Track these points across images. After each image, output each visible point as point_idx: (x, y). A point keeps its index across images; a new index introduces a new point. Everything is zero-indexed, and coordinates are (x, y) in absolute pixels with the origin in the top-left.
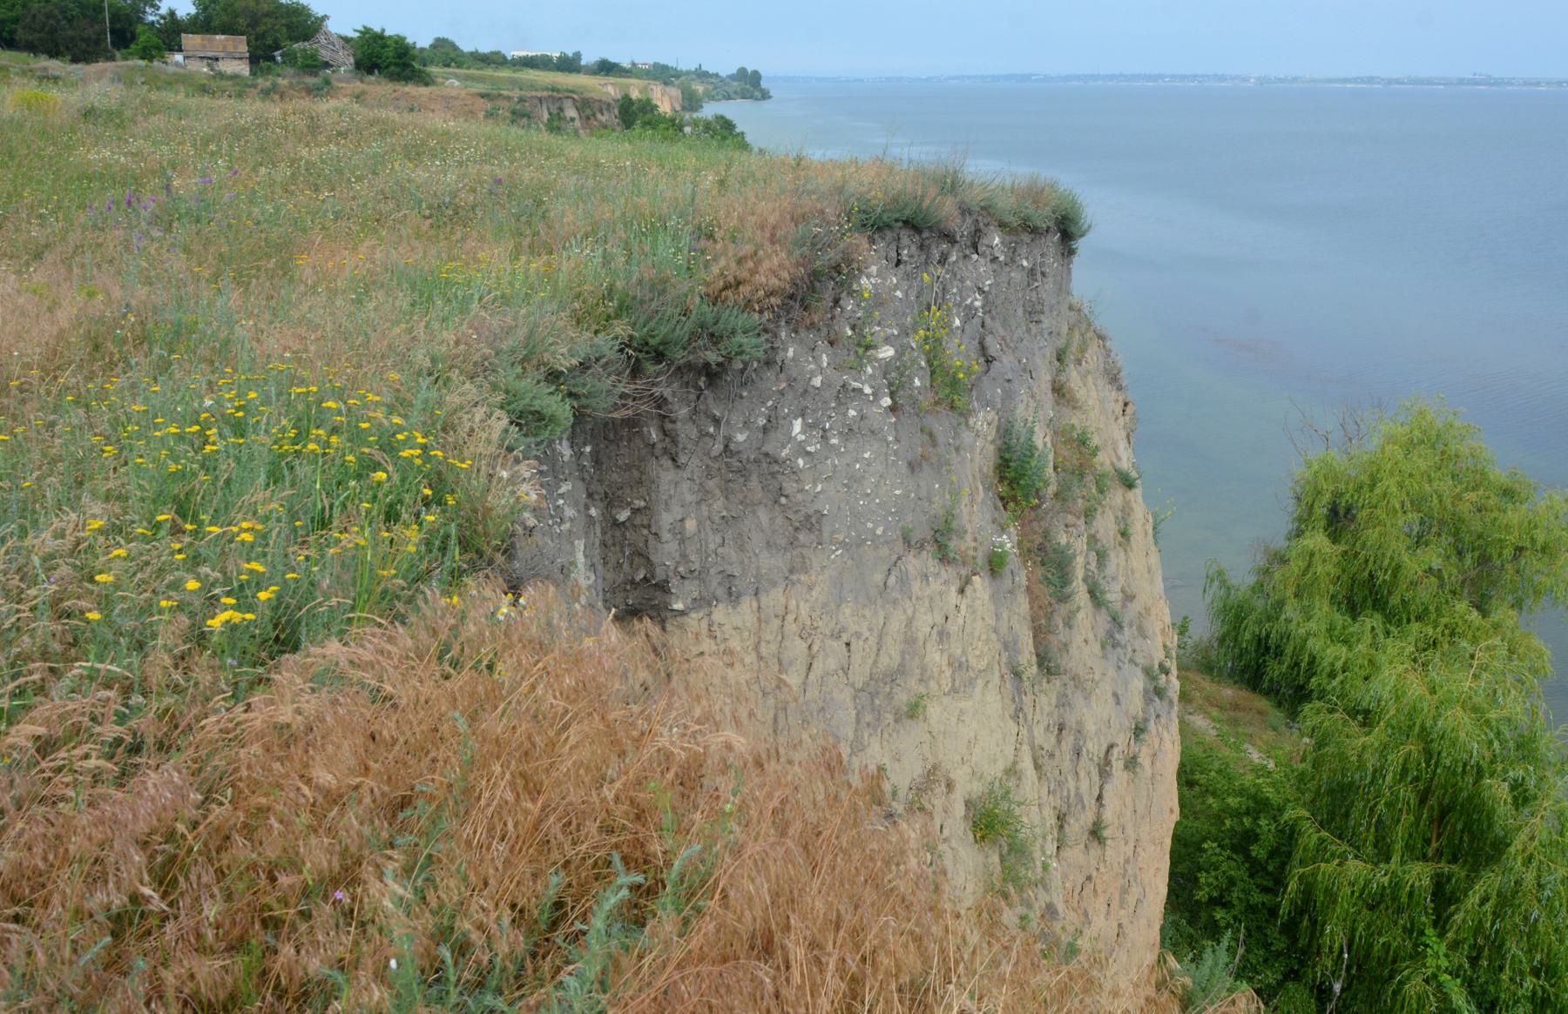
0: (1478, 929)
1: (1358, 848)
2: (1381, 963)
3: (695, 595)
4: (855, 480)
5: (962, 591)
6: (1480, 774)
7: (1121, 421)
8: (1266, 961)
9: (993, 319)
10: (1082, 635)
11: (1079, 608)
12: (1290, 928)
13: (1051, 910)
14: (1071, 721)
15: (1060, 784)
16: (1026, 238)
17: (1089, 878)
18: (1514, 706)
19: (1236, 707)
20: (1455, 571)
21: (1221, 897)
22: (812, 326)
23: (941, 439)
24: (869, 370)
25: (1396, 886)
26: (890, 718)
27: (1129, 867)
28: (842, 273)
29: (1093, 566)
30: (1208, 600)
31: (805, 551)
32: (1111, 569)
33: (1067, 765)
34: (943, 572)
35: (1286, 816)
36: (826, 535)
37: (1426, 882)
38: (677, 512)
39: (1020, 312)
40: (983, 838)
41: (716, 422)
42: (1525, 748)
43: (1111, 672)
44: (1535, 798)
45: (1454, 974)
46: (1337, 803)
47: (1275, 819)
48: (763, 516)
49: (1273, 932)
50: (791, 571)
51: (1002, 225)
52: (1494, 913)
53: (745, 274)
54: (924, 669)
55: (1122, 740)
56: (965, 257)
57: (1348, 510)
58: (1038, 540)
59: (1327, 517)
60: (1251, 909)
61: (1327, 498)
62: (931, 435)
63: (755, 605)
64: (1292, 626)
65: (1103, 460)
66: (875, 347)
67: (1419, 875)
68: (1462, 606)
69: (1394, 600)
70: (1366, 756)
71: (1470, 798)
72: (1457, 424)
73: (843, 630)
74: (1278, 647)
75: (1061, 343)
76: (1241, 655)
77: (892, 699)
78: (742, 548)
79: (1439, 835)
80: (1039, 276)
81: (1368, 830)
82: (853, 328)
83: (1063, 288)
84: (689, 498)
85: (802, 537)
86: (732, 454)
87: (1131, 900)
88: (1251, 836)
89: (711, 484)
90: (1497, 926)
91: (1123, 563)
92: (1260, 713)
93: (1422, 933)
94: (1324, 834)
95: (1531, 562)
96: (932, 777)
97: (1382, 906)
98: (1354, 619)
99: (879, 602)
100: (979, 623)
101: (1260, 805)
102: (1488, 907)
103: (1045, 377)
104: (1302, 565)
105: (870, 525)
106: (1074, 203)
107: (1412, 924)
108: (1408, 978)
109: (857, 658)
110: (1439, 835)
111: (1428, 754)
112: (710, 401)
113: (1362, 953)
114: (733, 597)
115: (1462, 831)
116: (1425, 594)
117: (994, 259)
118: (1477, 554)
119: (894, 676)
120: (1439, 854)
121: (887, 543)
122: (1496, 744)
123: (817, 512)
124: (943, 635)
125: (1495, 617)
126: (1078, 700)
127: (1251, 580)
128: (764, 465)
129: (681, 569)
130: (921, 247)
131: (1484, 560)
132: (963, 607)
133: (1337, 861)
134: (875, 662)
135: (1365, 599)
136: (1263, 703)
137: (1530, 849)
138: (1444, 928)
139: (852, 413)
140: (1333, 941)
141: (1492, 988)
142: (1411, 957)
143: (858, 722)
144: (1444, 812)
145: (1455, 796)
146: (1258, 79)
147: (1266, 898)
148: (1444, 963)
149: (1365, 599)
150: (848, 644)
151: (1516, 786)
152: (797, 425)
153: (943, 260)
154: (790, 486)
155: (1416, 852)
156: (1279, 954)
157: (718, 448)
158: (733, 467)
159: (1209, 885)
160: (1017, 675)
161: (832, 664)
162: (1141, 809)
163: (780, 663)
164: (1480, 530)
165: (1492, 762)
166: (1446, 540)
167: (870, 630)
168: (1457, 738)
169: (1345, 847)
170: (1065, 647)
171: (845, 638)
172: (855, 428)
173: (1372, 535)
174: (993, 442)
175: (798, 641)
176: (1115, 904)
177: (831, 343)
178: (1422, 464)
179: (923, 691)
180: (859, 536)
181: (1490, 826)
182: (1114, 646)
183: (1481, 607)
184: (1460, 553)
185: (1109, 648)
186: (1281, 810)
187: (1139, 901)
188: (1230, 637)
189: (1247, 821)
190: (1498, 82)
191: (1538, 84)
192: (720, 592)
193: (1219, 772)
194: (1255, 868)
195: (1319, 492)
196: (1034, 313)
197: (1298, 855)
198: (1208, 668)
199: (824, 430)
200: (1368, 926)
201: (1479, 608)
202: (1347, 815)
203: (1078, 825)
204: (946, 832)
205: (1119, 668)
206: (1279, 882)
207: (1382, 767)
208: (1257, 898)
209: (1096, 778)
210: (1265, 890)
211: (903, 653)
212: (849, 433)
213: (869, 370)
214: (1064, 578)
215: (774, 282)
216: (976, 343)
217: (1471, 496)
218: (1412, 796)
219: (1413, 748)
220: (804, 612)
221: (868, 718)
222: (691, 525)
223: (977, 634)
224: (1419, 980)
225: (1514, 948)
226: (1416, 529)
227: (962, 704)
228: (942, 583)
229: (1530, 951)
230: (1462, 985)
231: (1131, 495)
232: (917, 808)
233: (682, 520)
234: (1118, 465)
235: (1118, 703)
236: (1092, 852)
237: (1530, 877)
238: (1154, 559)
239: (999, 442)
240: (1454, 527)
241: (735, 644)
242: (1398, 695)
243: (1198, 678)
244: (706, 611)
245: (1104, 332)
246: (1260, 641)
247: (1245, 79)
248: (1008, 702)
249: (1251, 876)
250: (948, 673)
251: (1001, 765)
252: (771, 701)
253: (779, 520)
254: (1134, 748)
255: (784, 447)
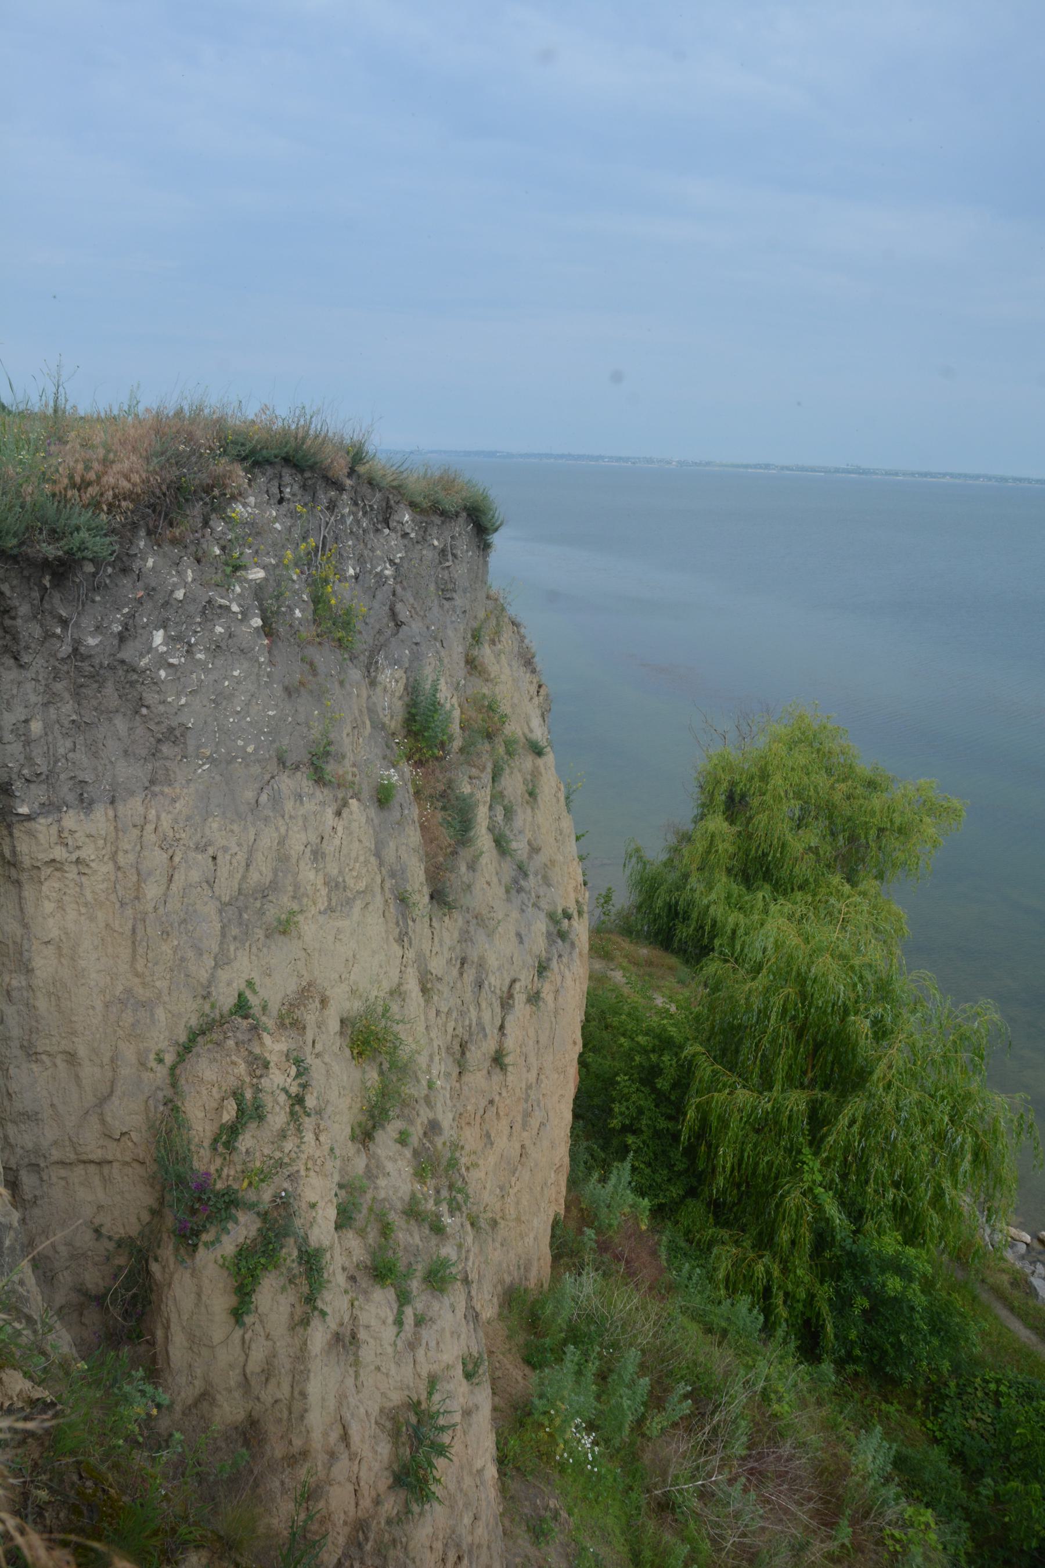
0: (847, 1149)
1: (746, 1080)
2: (766, 1179)
3: (43, 799)
4: (221, 699)
5: (338, 814)
6: (846, 1012)
7: (536, 700)
8: (669, 1180)
9: (404, 589)
10: (485, 878)
11: (482, 853)
12: (690, 1152)
13: (433, 1127)
14: (474, 956)
15: (462, 1014)
16: (437, 520)
17: (491, 1102)
18: (874, 953)
19: (650, 963)
20: (829, 848)
21: (632, 1125)
22: (174, 542)
23: (322, 669)
24: (238, 589)
25: (777, 1111)
26: (260, 933)
27: (532, 1093)
28: (215, 497)
29: (500, 818)
30: (628, 872)
31: (168, 764)
32: (519, 822)
33: (468, 996)
34: (318, 793)
35: (685, 1052)
36: (191, 749)
37: (803, 1107)
38: (20, 713)
39: (432, 587)
40: (360, 1054)
41: (64, 623)
42: (884, 990)
43: (515, 914)
44: (892, 1032)
45: (828, 1188)
46: (728, 1042)
47: (676, 1054)
48: (121, 724)
49: (676, 1154)
50: (152, 782)
51: (413, 505)
52: (860, 1133)
53: (91, 476)
54: (296, 886)
55: (526, 978)
56: (377, 530)
57: (743, 796)
58: (441, 787)
59: (726, 803)
60: (657, 1134)
61: (725, 785)
62: (311, 664)
63: (111, 813)
64: (697, 895)
65: (513, 729)
66: (245, 568)
67: (797, 1101)
68: (836, 879)
69: (784, 873)
70: (753, 999)
71: (838, 1033)
72: (829, 726)
73: (209, 843)
74: (685, 912)
75: (476, 624)
76: (655, 920)
77: (260, 913)
78: (96, 755)
79: (813, 1066)
80: (450, 557)
81: (754, 1063)
82: (223, 548)
83: (479, 575)
84: (33, 698)
85: (165, 749)
86: (84, 658)
87: (534, 1123)
88: (655, 1071)
89: (59, 686)
90: (863, 1144)
91: (530, 819)
92: (671, 968)
93: (799, 1152)
94: (717, 1067)
95: (892, 842)
96: (308, 993)
97: (766, 1129)
98: (748, 889)
99: (250, 818)
100: (356, 845)
101: (665, 1043)
102: (855, 1128)
103: (457, 650)
104: (706, 844)
105: (240, 743)
106: (485, 498)
107: (792, 1145)
108: (789, 1192)
109: (223, 872)
110: (813, 1066)
111: (803, 995)
112: (56, 601)
113: (750, 1172)
114: (86, 804)
115: (833, 1063)
116: (804, 869)
117: (405, 535)
118: (847, 834)
119: (264, 893)
120: (813, 1081)
121: (259, 761)
122: (859, 986)
123: (181, 725)
124: (317, 855)
125: (861, 887)
126: (480, 937)
127: (664, 857)
128: (120, 672)
129: (25, 772)
130: (304, 487)
131: (852, 839)
132: (340, 829)
133: (727, 1091)
134: (244, 877)
135: (756, 872)
136: (673, 960)
137: (889, 1076)
138: (819, 1148)
139: (219, 629)
140: (725, 1161)
141: (859, 1199)
142: (791, 1174)
143: (223, 935)
144: (818, 1046)
145: (826, 1033)
146: (678, 462)
147: (670, 1125)
148: (819, 1178)
149: (756, 872)
150: (214, 858)
151: (877, 1022)
152: (159, 637)
153: (332, 507)
154: (151, 697)
155: (791, 1082)
156: (680, 1174)
157: (65, 649)
158: (82, 672)
159: (622, 1114)
160: (403, 900)
161: (195, 876)
162: (544, 1039)
163: (139, 874)
164: (849, 814)
165: (856, 1002)
166: (822, 824)
167: (239, 845)
168: (827, 981)
169: (735, 1078)
170: (469, 887)
171: (211, 851)
172: (223, 645)
173: (761, 819)
174: (400, 698)
175: (157, 851)
176: (517, 1126)
177: (199, 561)
178: (802, 761)
179: (296, 907)
180: (229, 753)
181: (854, 1056)
182: (518, 892)
183: (851, 879)
184: (832, 834)
185: (513, 892)
186: (681, 1047)
187: (542, 1124)
188: (645, 905)
189: (654, 1057)
190: (865, 472)
191: (897, 474)
192: (71, 798)
193: (629, 1015)
194: (661, 1099)
195: (718, 782)
196: (446, 592)
197: (695, 1086)
198: (628, 931)
199: (190, 645)
200: (755, 1145)
201: (849, 880)
202: (737, 1051)
203: (479, 1053)
204: (319, 1047)
205: (523, 911)
206: (677, 1113)
207: (766, 1008)
208: (663, 1124)
209: (498, 1010)
210: (669, 1118)
211: (275, 872)
212: (217, 649)
213: (238, 589)
214: (464, 826)
215: (125, 485)
216: (387, 608)
217: (842, 786)
218: (791, 1032)
219: (790, 990)
220: (166, 822)
221: (235, 931)
222: (36, 727)
223: (353, 855)
224: (797, 1193)
225: (877, 1164)
226: (797, 813)
227: (339, 924)
228: (317, 804)
229: (891, 1166)
230: (834, 1196)
231: (540, 762)
232: (291, 1022)
233: (26, 721)
234: (529, 735)
235: (521, 942)
236: (495, 1078)
237: (889, 1100)
238: (567, 824)
239: (406, 699)
240: (829, 811)
241: (88, 852)
242: (778, 946)
243: (619, 940)
244: (56, 816)
245: (518, 620)
246: (670, 907)
247: (668, 463)
248: (392, 925)
249: (657, 1106)
250: (324, 892)
251: (386, 986)
252: (129, 912)
253: (140, 731)
254: (537, 984)
255: (142, 656)
